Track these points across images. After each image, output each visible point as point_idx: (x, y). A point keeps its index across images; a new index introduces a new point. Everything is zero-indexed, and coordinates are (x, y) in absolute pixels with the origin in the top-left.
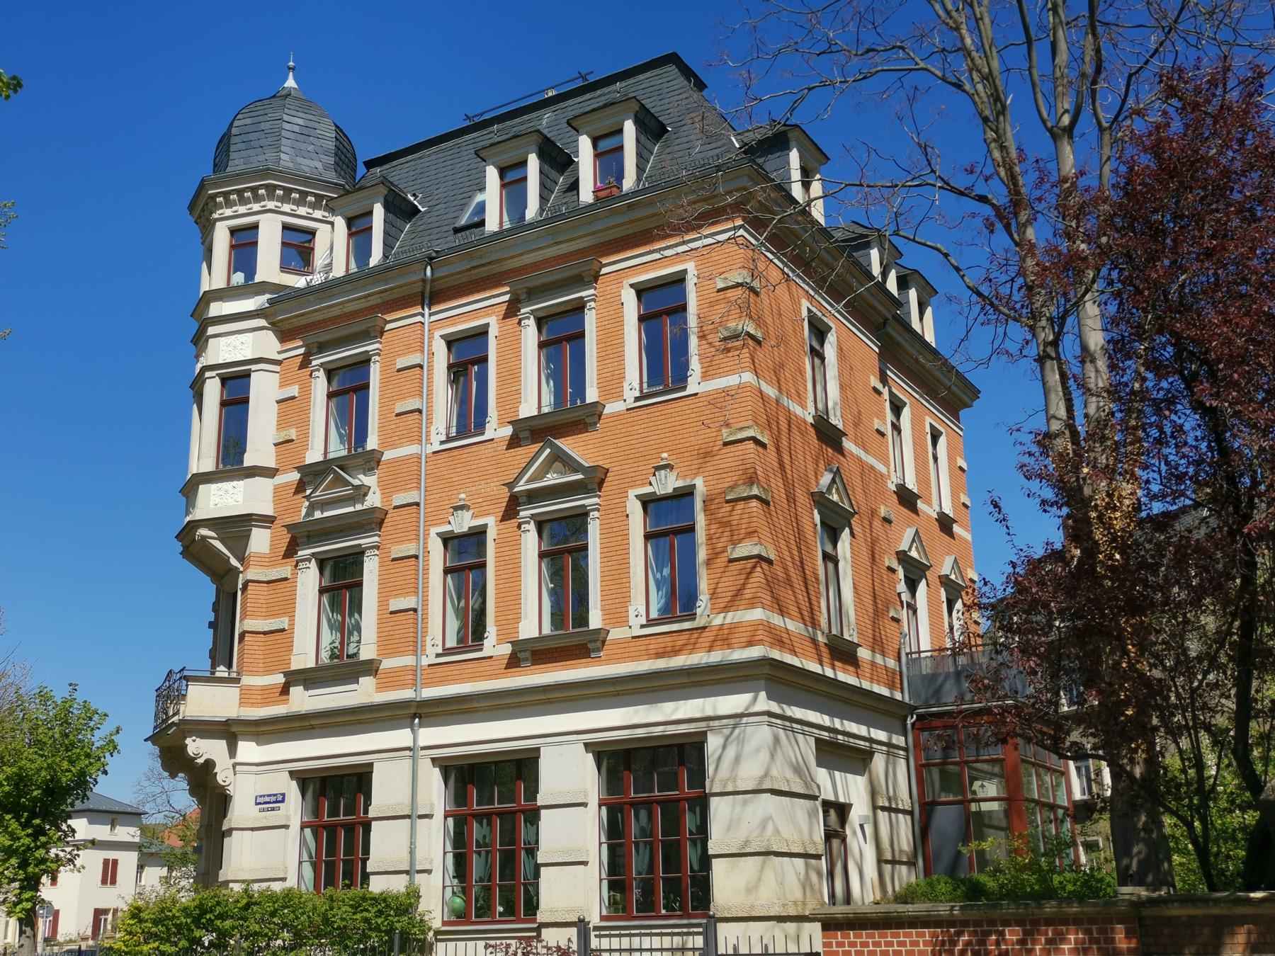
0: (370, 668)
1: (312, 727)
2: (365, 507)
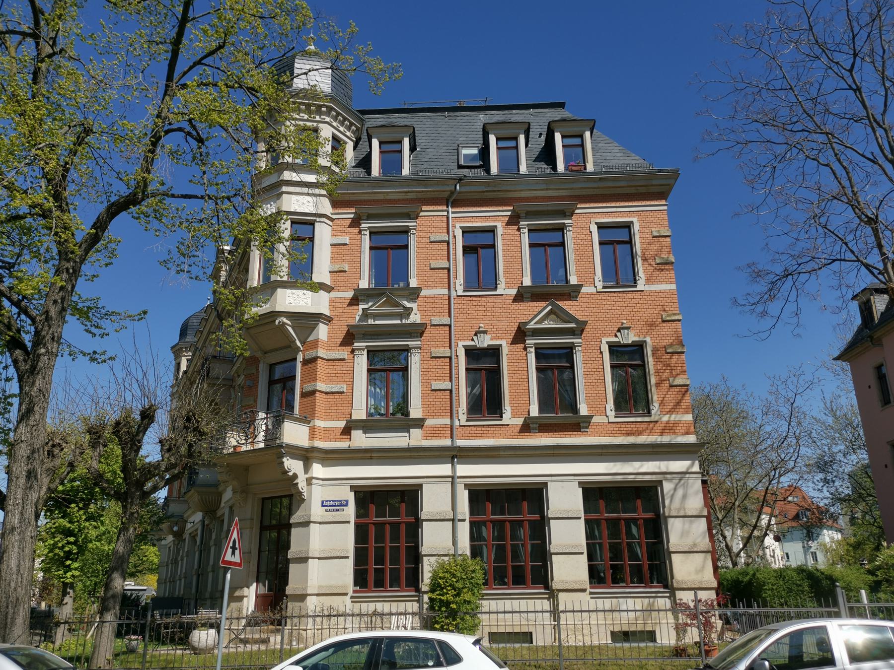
0: (419, 423)
1: (371, 458)
2: (409, 322)
